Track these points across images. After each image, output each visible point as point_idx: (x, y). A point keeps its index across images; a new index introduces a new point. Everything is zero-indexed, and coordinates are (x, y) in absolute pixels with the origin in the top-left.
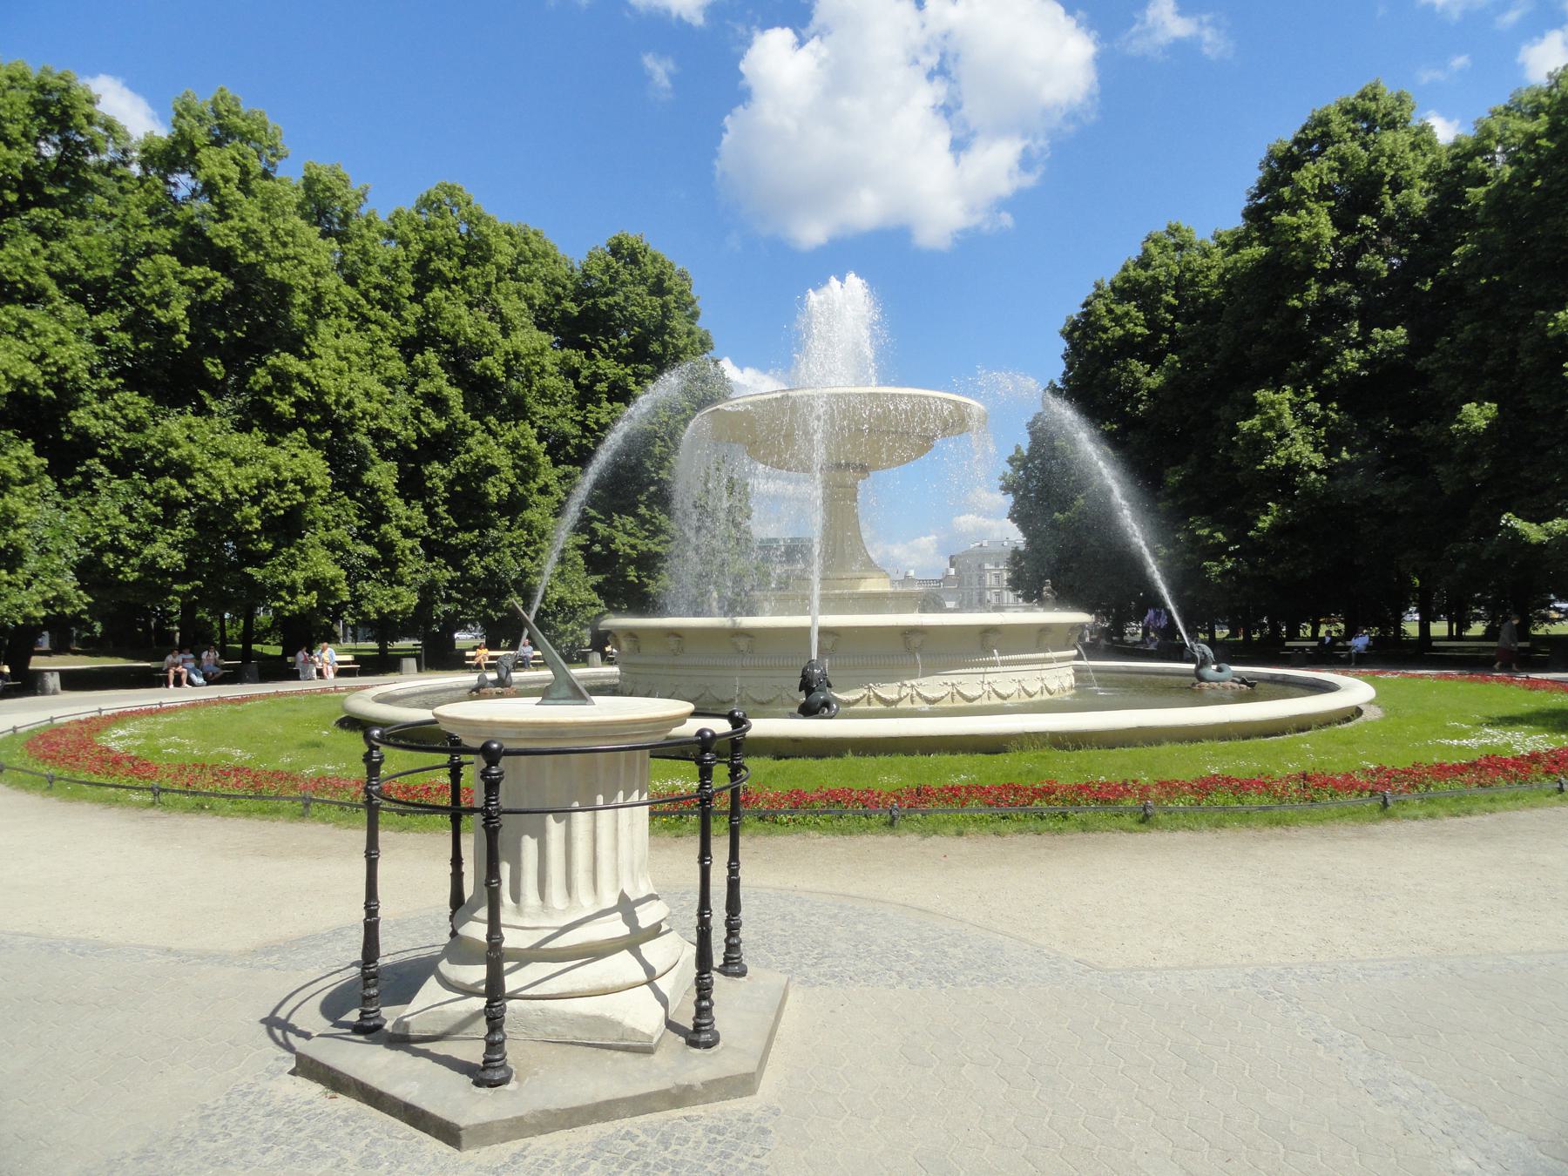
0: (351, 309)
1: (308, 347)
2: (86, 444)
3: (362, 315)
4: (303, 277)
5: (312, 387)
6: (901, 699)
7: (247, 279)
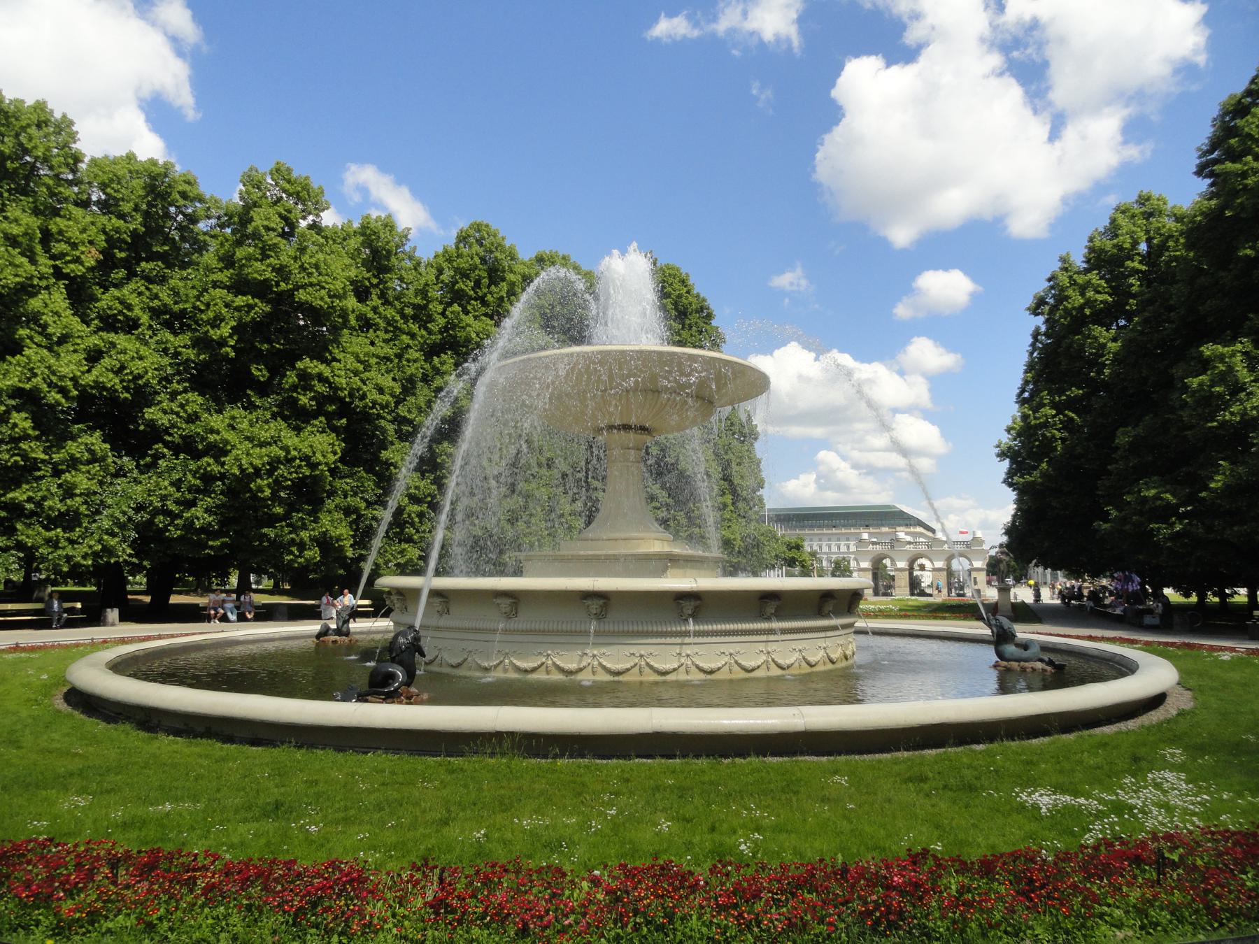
0: (389, 323)
1: (331, 353)
2: (155, 433)
3: (396, 328)
4: (322, 299)
5: (330, 384)
6: (580, 670)
7: (284, 304)
